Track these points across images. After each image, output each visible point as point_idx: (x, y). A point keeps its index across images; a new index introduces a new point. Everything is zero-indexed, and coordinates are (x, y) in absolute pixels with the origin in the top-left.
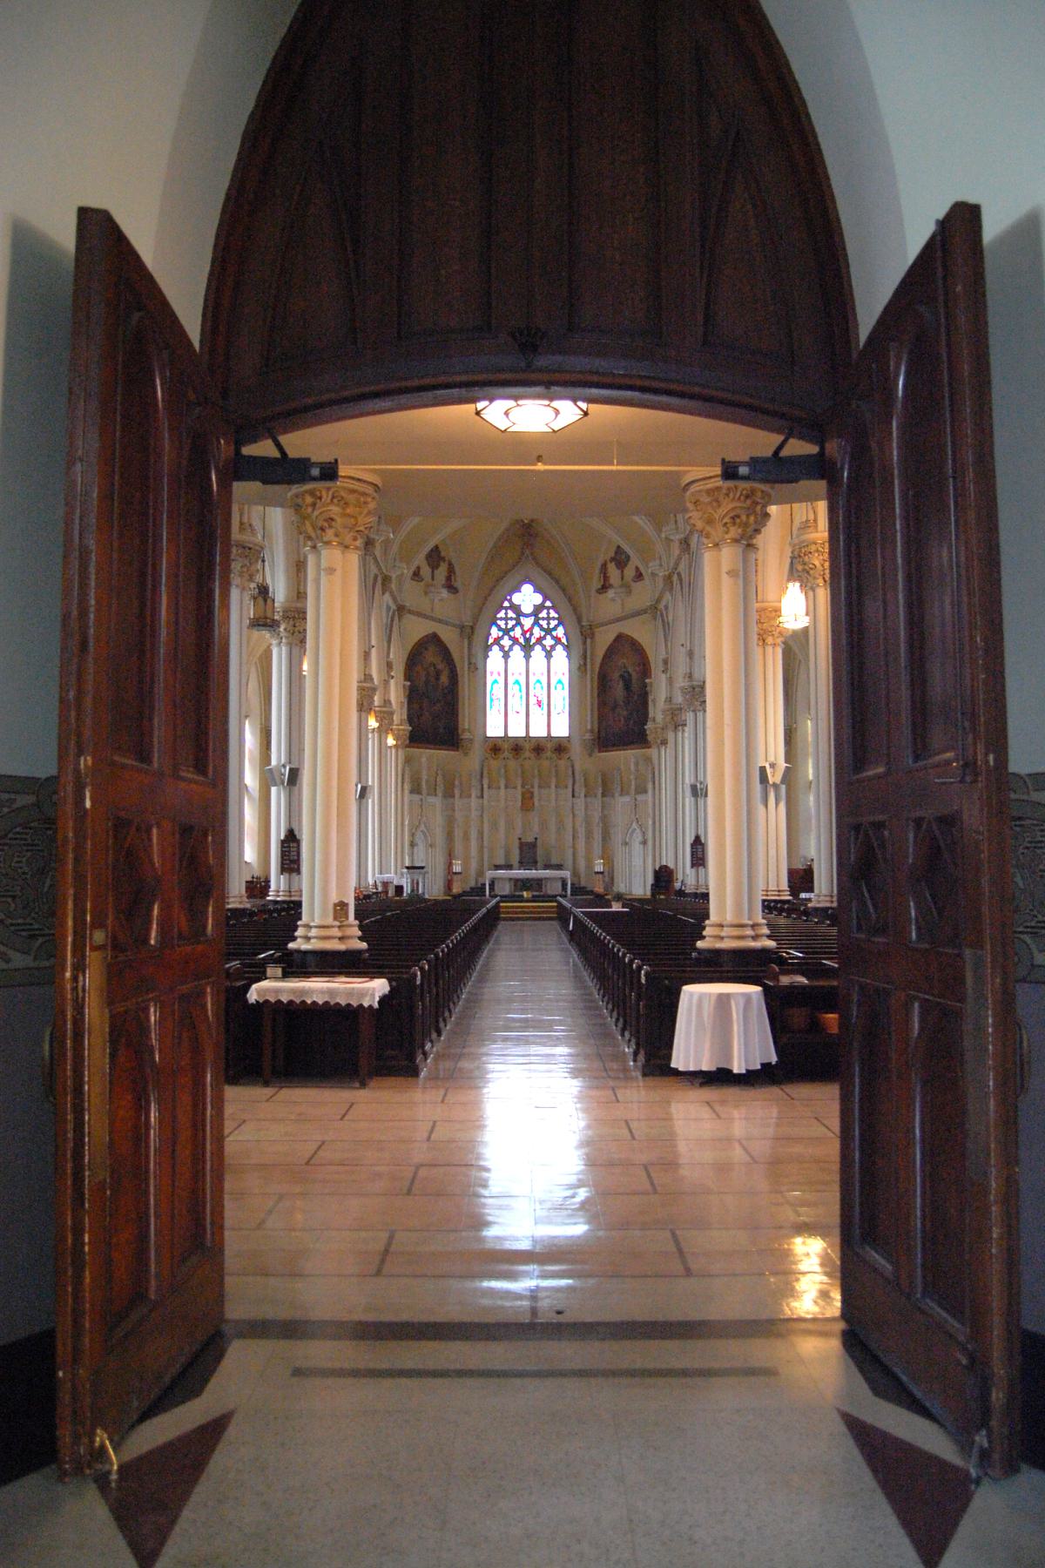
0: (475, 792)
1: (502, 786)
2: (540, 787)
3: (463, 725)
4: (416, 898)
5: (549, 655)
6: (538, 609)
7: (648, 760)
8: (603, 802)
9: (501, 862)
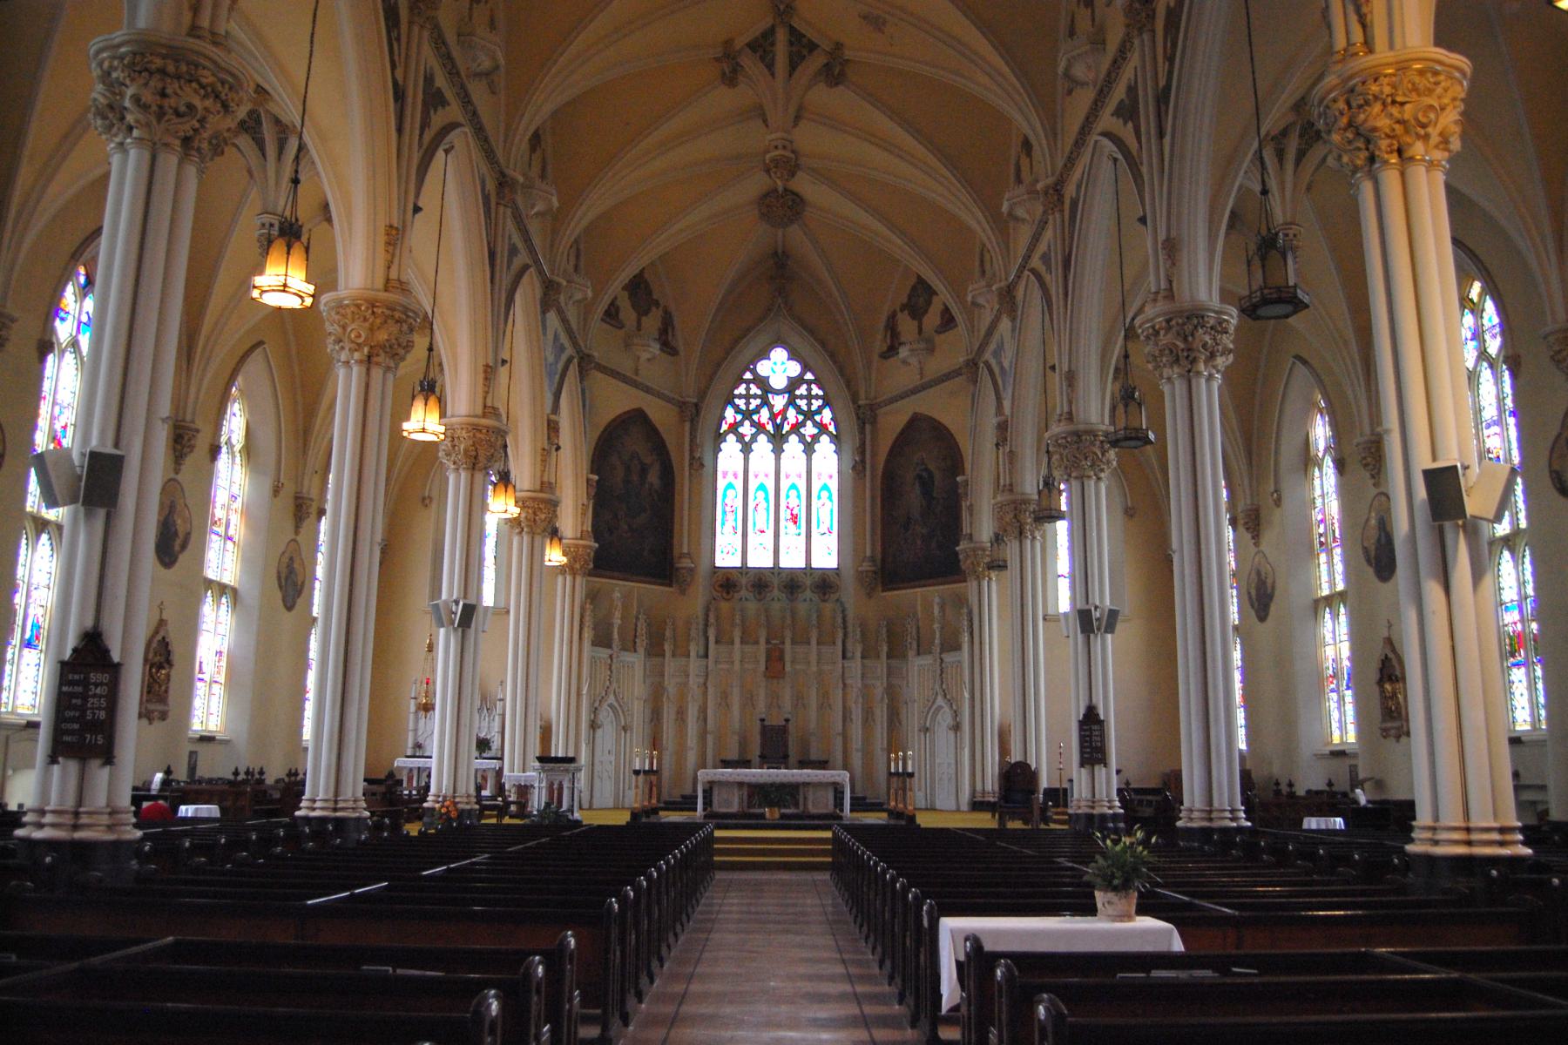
0: (694, 649)
1: (737, 640)
2: (794, 642)
3: (681, 545)
4: (556, 824)
5: (809, 449)
6: (794, 383)
7: (961, 601)
8: (889, 667)
9: (733, 755)
